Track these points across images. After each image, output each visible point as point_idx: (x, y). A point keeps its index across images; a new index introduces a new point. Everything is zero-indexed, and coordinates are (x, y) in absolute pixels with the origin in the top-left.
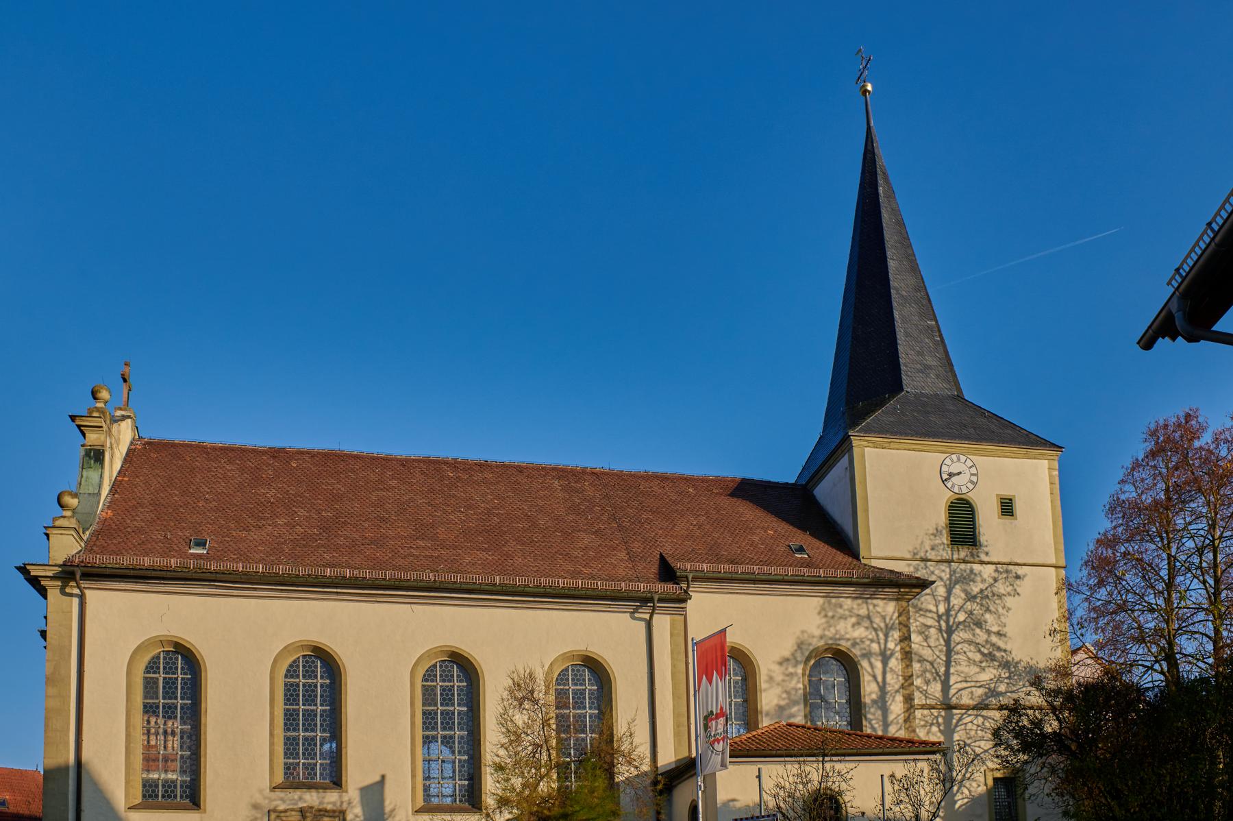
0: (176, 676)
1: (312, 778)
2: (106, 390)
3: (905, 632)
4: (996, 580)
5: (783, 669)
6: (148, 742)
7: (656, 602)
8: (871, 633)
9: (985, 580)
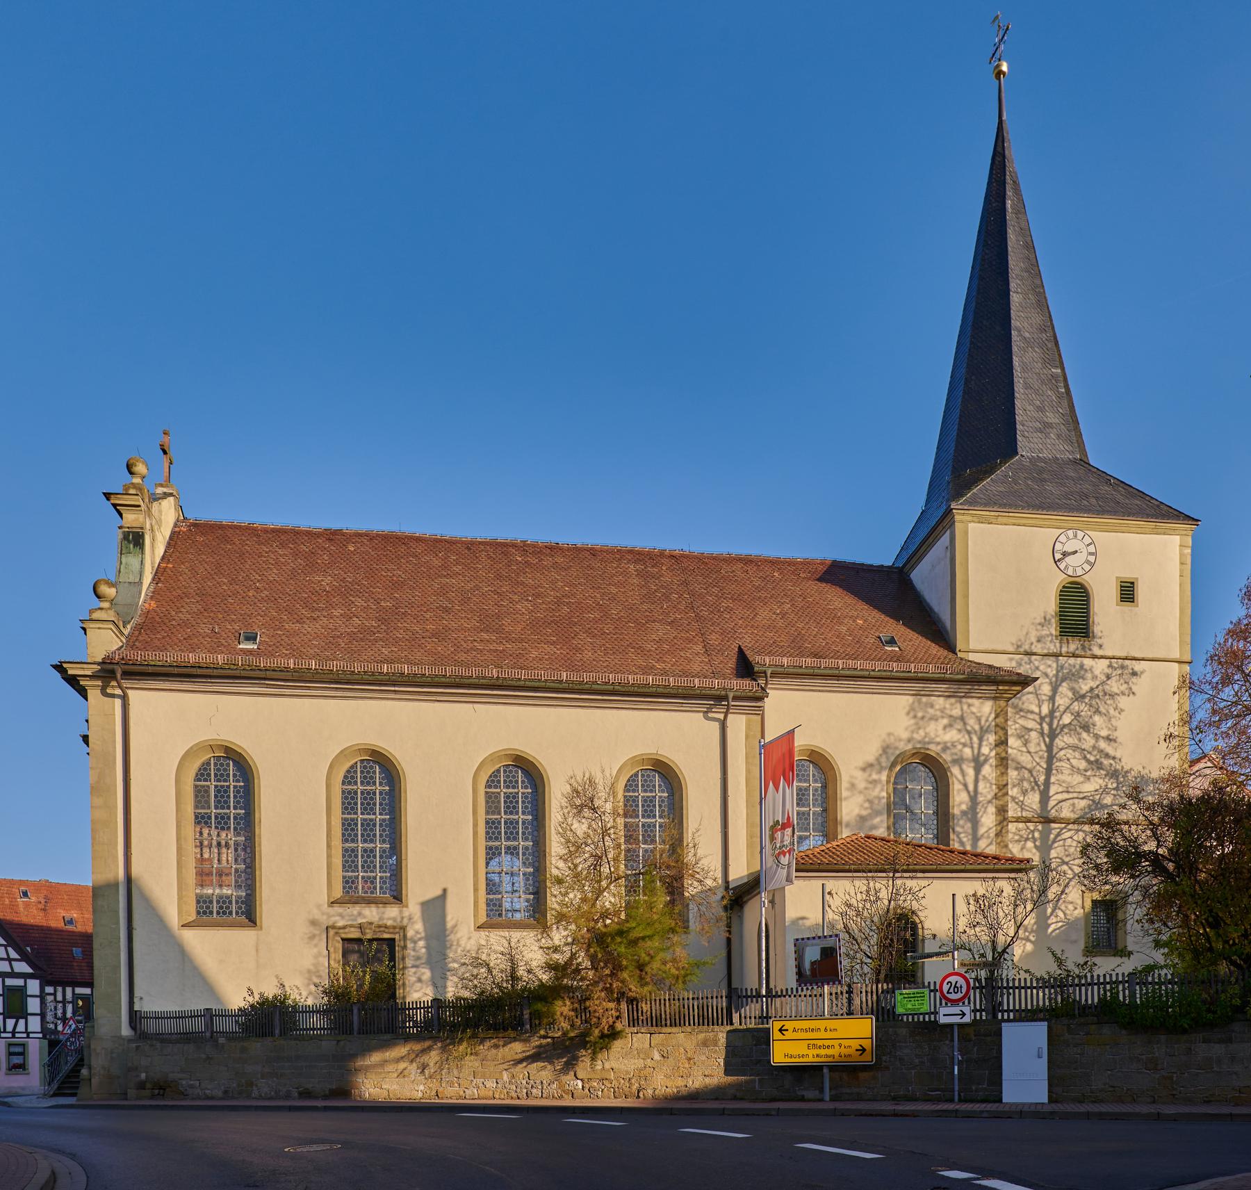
0: (228, 784)
1: (372, 893)
2: (143, 463)
3: (1002, 735)
4: (1108, 677)
5: (866, 775)
6: (202, 855)
7: (730, 700)
8: (964, 737)
9: (1097, 677)
